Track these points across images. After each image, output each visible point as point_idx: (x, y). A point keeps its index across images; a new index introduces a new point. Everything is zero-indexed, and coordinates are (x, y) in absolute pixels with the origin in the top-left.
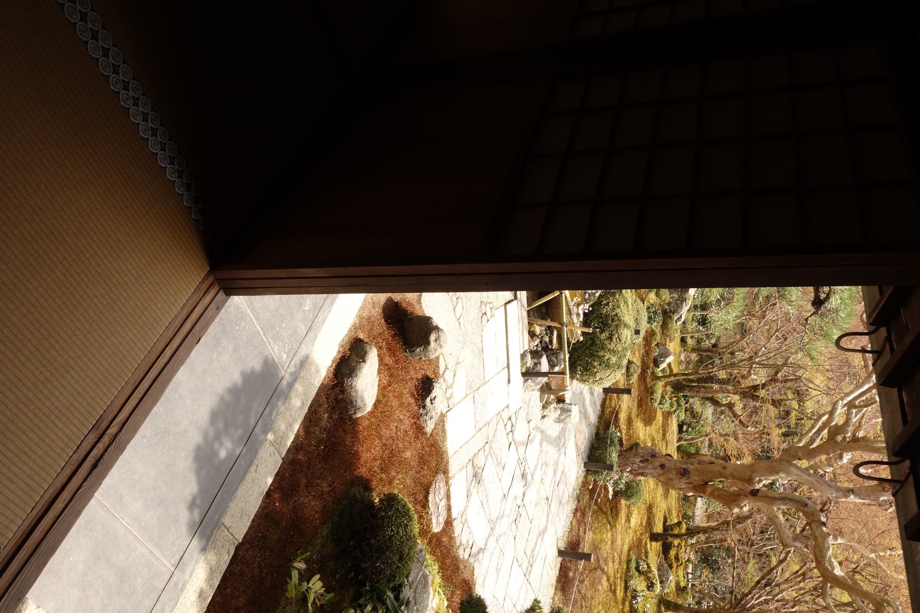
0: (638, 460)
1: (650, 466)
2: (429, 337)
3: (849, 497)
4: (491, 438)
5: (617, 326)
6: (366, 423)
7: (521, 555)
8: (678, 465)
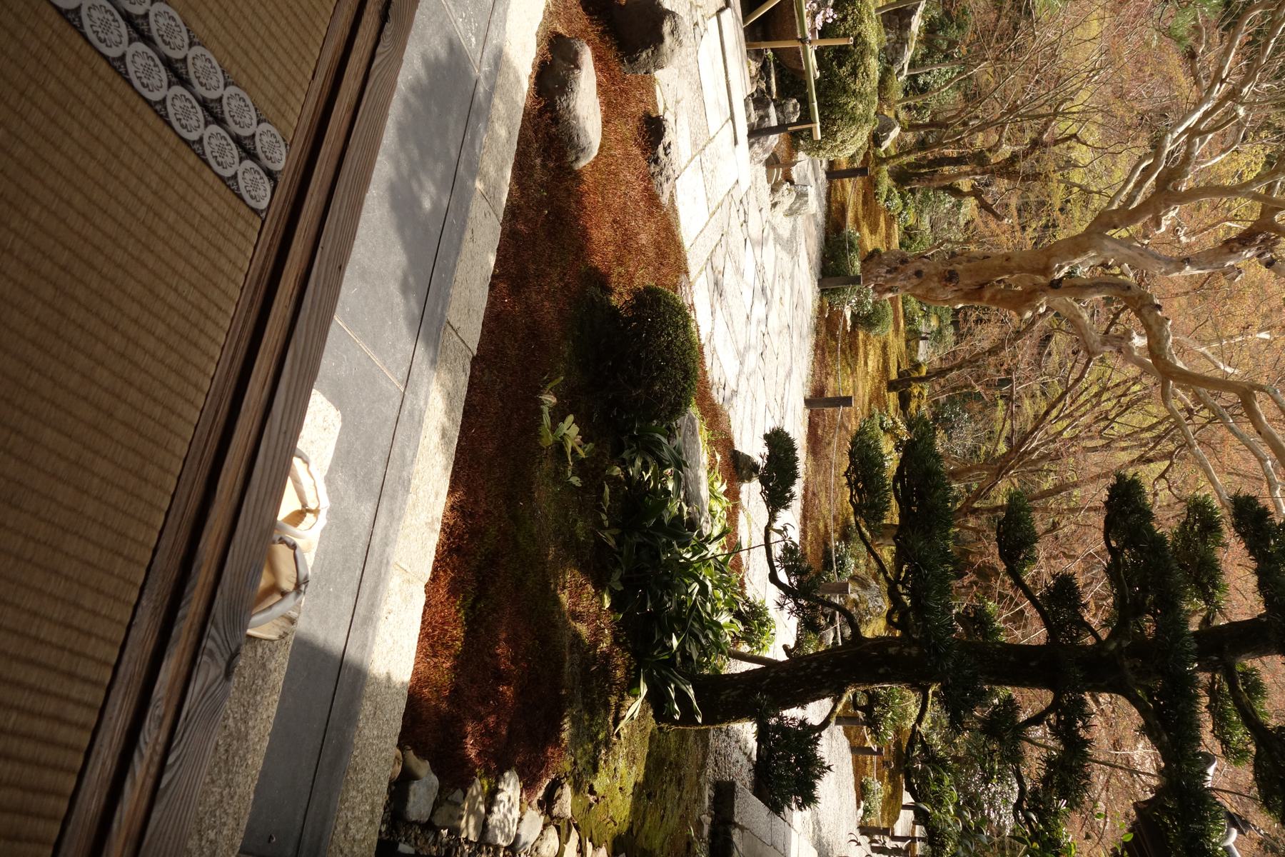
1: (901, 277)
2: (661, 28)
4: (725, 229)
5: (861, 53)
6: (587, 178)
7: (772, 404)
8: (940, 267)
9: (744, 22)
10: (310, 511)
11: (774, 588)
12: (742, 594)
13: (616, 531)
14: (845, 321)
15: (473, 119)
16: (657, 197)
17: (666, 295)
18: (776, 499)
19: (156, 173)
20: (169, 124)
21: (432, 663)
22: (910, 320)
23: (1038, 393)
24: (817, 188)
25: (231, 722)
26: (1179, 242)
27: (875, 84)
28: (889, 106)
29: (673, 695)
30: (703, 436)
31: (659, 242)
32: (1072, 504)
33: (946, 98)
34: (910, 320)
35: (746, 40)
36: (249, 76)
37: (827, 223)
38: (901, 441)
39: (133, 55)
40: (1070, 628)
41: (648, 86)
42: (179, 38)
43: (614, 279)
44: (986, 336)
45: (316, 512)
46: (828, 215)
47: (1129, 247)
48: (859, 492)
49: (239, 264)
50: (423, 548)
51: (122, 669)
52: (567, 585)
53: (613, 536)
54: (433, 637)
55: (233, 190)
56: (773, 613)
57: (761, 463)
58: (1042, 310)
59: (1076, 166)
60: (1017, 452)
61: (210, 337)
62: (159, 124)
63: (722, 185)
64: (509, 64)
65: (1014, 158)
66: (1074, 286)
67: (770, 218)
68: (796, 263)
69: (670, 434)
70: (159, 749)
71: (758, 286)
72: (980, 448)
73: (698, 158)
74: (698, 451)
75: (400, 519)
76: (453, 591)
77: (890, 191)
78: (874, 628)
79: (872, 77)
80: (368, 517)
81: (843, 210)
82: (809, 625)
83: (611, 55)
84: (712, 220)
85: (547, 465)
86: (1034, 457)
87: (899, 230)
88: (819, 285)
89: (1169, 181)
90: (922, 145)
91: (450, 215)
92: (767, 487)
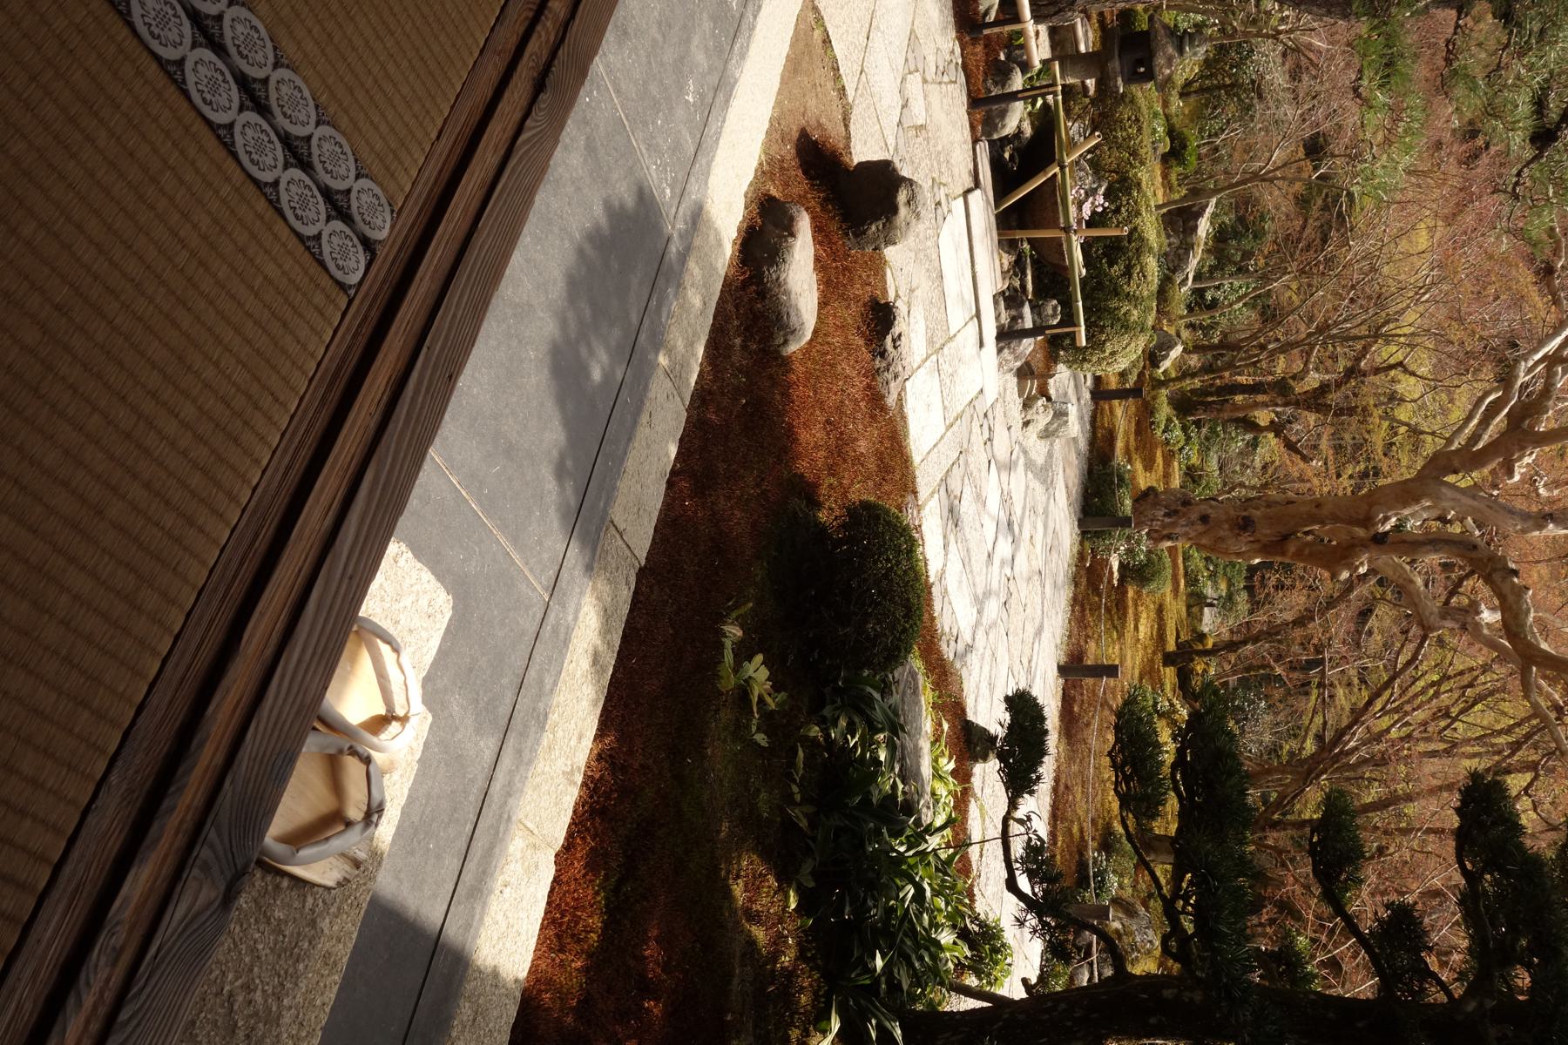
0: (1160, 513)
3: (1545, 527)
4: (965, 446)
5: (1137, 250)
6: (799, 369)
7: (1017, 667)
9: (997, 206)
10: (396, 718)
11: (1012, 899)
12: (971, 908)
13: (809, 809)
14: (1111, 573)
15: (661, 282)
16: (883, 397)
17: (887, 512)
18: (1019, 782)
19: (209, 213)
20: (235, 156)
21: (558, 961)
22: (1192, 580)
23: (1356, 681)
24: (1080, 410)
25: (258, 997)
26: (1538, 495)
27: (1154, 287)
28: (1169, 321)
29: (874, 1035)
30: (926, 697)
31: (882, 453)
32: (1403, 825)
33: (1240, 317)
34: (1192, 580)
35: (998, 229)
36: (351, 120)
37: (1091, 451)
38: (1180, 729)
39: (196, 63)
40: (1411, 979)
41: (878, 266)
42: (261, 53)
43: (823, 491)
44: (1288, 605)
45: (404, 720)
46: (1092, 442)
47: (1474, 497)
48: (1127, 779)
49: (311, 347)
50: (556, 804)
51: (67, 870)
52: (743, 873)
53: (806, 815)
54: (561, 924)
55: (313, 254)
56: (1010, 933)
57: (1000, 732)
58: (1362, 570)
59: (1402, 400)
60: (1331, 750)
61: (258, 435)
62: (220, 154)
63: (965, 391)
64: (709, 224)
65: (1324, 388)
66: (1404, 542)
67: (1021, 438)
68: (1051, 496)
69: (885, 689)
70: (109, 996)
71: (1004, 519)
72: (1281, 748)
73: (934, 358)
74: (920, 715)
75: (530, 762)
76: (592, 865)
77: (1169, 420)
78: (1144, 966)
79: (1150, 278)
80: (488, 755)
81: (1111, 437)
82: (1057, 951)
83: (834, 226)
84: (949, 434)
85: (726, 716)
86: (1353, 760)
87: (1180, 469)
88: (1080, 526)
89: (1523, 419)
90: (1207, 369)
91: (624, 394)
92: (1007, 765)
